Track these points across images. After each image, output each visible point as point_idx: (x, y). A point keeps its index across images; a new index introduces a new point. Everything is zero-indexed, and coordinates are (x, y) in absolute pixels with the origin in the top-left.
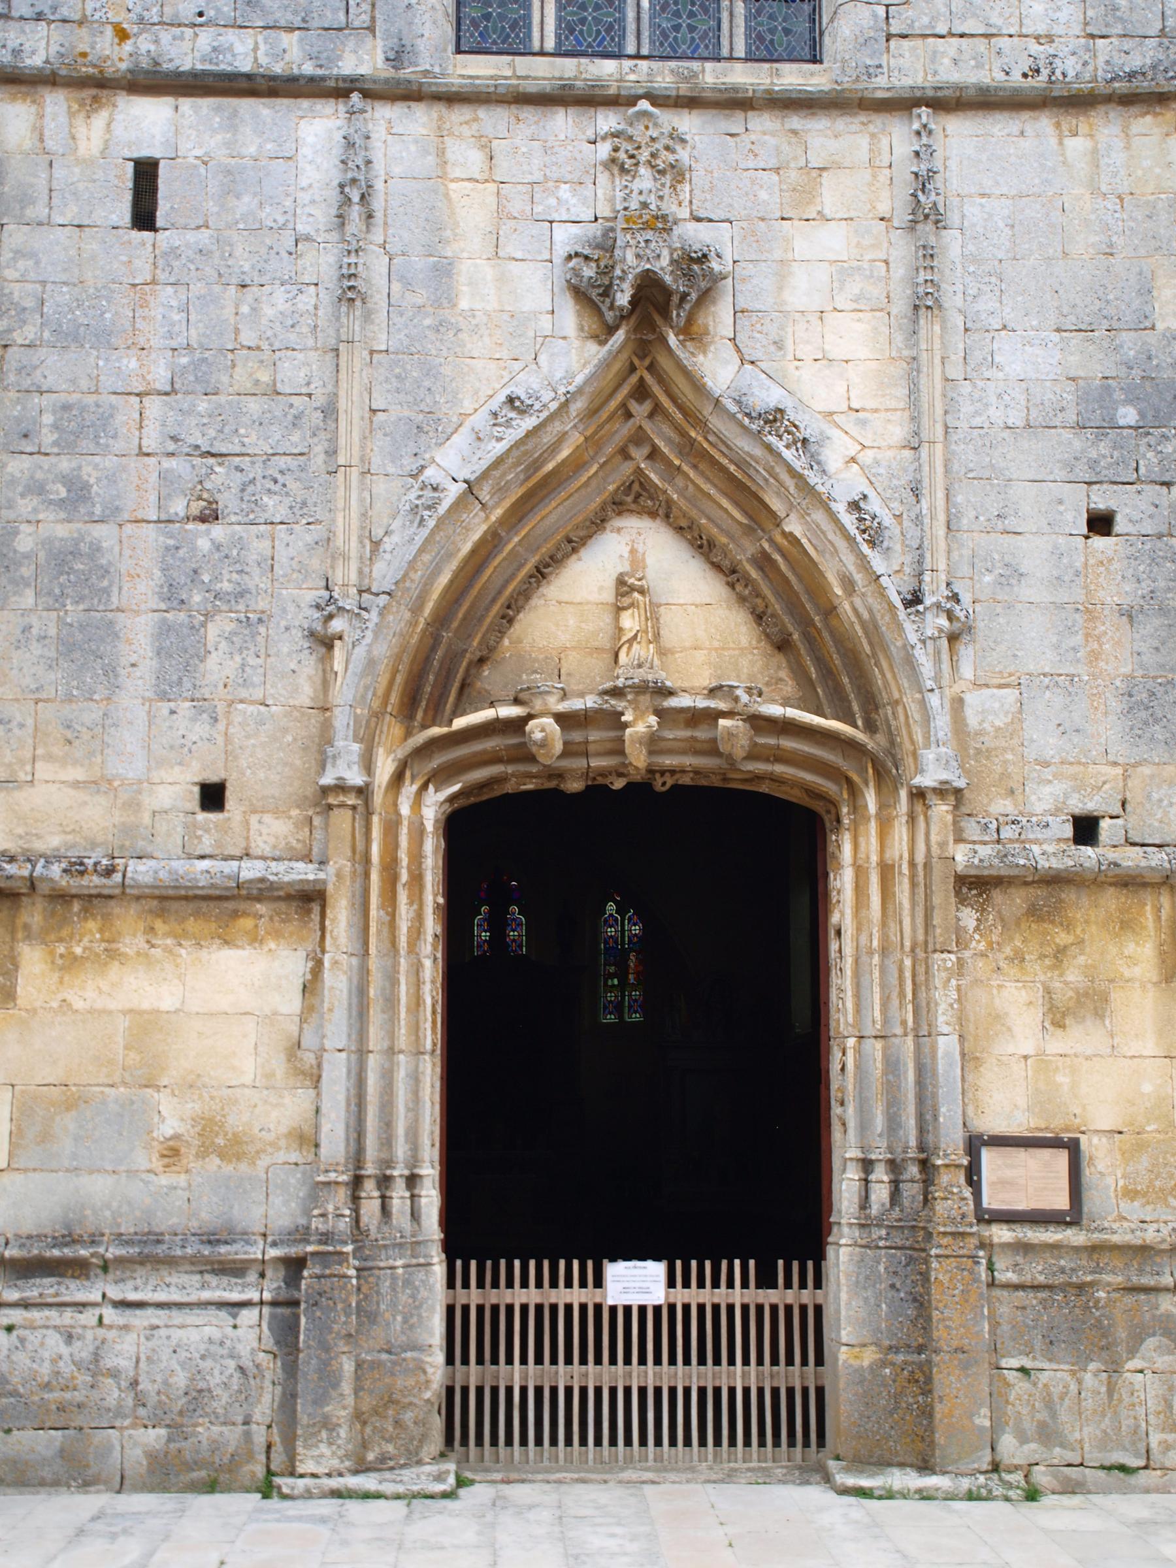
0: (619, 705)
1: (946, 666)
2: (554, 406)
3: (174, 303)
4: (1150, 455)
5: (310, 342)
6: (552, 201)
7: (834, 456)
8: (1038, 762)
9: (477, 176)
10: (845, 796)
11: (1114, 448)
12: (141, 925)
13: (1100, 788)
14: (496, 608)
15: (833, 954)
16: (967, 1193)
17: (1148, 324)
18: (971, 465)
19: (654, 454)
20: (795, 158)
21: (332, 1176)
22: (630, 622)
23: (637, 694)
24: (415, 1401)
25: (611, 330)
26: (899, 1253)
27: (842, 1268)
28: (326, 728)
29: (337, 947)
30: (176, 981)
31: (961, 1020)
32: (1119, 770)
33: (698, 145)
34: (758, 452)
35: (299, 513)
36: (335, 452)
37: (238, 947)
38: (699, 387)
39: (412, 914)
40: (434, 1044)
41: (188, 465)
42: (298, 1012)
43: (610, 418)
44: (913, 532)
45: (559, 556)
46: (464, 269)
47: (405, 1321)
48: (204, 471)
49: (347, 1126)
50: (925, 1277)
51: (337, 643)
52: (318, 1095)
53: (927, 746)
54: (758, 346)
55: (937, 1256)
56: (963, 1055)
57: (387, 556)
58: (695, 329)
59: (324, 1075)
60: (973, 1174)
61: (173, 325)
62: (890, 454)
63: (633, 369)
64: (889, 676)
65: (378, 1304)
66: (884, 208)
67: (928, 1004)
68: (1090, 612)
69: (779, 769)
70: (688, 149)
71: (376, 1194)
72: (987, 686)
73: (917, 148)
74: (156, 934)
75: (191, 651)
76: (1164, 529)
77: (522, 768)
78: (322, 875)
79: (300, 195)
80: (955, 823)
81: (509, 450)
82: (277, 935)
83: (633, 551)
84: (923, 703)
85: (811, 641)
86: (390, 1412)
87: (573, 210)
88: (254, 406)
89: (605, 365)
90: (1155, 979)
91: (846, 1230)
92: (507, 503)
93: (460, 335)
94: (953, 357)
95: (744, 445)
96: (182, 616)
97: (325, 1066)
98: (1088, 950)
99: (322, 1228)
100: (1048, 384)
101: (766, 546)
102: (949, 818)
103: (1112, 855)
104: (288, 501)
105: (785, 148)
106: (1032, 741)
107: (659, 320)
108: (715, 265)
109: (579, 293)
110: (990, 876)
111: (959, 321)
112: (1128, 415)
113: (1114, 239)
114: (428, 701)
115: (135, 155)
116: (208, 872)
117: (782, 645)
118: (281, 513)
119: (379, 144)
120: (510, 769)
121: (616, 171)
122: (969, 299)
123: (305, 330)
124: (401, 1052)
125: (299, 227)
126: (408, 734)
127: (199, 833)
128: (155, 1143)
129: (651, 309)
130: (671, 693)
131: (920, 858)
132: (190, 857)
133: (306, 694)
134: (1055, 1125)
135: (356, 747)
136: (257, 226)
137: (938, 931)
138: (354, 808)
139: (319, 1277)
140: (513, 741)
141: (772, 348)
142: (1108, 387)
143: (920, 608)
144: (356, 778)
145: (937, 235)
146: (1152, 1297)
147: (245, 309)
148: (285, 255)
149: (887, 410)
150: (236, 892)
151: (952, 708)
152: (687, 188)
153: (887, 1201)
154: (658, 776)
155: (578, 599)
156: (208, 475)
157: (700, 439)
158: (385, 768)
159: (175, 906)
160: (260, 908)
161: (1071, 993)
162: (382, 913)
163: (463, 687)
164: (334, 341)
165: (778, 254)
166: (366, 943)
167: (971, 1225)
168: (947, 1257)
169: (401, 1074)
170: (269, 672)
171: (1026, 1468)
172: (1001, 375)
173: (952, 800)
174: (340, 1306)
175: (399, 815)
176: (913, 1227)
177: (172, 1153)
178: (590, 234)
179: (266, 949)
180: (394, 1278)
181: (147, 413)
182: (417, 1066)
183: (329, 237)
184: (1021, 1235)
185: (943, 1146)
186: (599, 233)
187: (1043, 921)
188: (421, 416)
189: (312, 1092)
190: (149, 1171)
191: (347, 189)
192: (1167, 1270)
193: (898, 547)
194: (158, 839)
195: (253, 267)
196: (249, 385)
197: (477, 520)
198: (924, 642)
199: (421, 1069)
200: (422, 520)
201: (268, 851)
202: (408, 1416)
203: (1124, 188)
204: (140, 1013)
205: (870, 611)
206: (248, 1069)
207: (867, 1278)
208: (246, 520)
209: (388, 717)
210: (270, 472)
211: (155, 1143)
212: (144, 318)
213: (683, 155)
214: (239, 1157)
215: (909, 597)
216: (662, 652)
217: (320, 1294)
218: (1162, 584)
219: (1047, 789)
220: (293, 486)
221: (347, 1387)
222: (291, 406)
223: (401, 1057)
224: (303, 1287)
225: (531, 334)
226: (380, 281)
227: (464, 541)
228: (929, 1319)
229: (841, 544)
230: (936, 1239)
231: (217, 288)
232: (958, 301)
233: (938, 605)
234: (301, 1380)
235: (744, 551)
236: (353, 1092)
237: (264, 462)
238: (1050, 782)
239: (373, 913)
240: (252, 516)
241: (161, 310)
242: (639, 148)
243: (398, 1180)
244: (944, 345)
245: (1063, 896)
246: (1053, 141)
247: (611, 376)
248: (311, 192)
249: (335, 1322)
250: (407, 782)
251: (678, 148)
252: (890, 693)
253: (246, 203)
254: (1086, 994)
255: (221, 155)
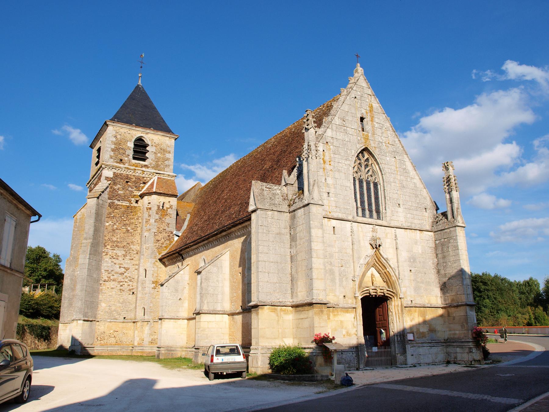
88: (345, 254)
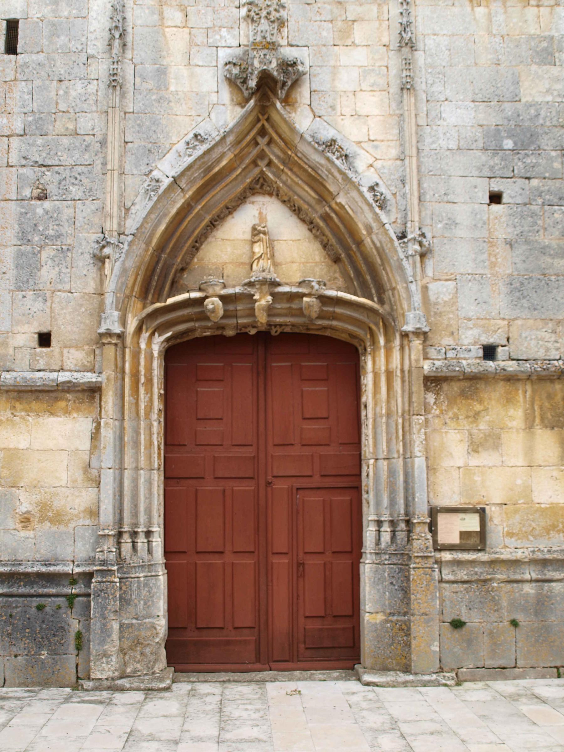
0: (252, 291)
1: (419, 269)
2: (218, 138)
3: (26, 90)
4: (520, 164)
5: (94, 108)
6: (218, 37)
7: (361, 164)
8: (465, 318)
9: (179, 25)
10: (369, 337)
11: (502, 160)
12: (9, 405)
13: (496, 331)
14: (189, 242)
15: (363, 417)
16: (429, 536)
17: (517, 99)
18: (431, 169)
19: (270, 164)
20: (340, 16)
21: (106, 532)
22: (258, 249)
23: (261, 285)
24: (151, 643)
25: (247, 100)
26: (395, 567)
27: (366, 574)
28: (102, 304)
29: (108, 416)
30: (27, 434)
31: (427, 450)
32: (506, 322)
33: (291, 9)
34: (323, 161)
35: (88, 194)
36: (106, 164)
37: (58, 416)
38: (292, 129)
39: (147, 399)
40: (159, 465)
41: (32, 172)
42: (89, 449)
43: (247, 145)
44: (402, 202)
45: (222, 216)
46: (172, 71)
47: (145, 604)
48: (40, 174)
49: (114, 507)
50: (408, 578)
51: (107, 260)
52: (99, 491)
53: (409, 311)
54: (322, 108)
55: (414, 568)
56: (428, 467)
57: (133, 216)
58: (290, 100)
59: (102, 481)
60: (433, 527)
61: (25, 101)
62: (390, 163)
63: (259, 120)
64: (390, 275)
65: (131, 595)
66: (385, 40)
67: (410, 441)
68: (490, 242)
69: (334, 323)
70: (286, 11)
71: (130, 540)
72: (440, 280)
73: (401, 11)
74: (16, 410)
75: (33, 266)
76: (527, 201)
77: (203, 324)
78: (99, 379)
79: (90, 35)
80: (424, 349)
81: (195, 161)
82: (78, 410)
83: (260, 213)
84: (407, 289)
85: (350, 257)
86: (138, 649)
87: (228, 41)
88: (65, 141)
89: (244, 118)
90: (523, 428)
91: (369, 556)
92: (194, 188)
93: (170, 104)
94: (421, 115)
95: (316, 158)
96: (29, 248)
97: (102, 476)
98: (490, 413)
99: (102, 558)
100: (469, 128)
101: (328, 209)
102: (421, 347)
103: (502, 364)
104: (82, 189)
105: (335, 11)
106: (463, 308)
107: (270, 93)
108: (300, 68)
109: (231, 81)
110: (441, 376)
111: (424, 97)
112: (509, 144)
113: (500, 57)
114: (155, 289)
115: (7, 17)
116: (42, 378)
117: (337, 260)
118: (79, 195)
119: (130, 10)
120: (197, 324)
121: (250, 21)
122: (429, 85)
123: (91, 102)
124: (142, 469)
125: (89, 51)
126: (144, 307)
127: (38, 358)
128: (18, 515)
129: (267, 90)
130: (279, 285)
131: (406, 368)
132: (33, 370)
133: (91, 287)
134: (474, 501)
135: (116, 314)
136: (68, 51)
137: (415, 404)
138: (116, 345)
139: (100, 582)
140: (197, 310)
141: (330, 110)
142: (499, 130)
143: (406, 240)
144: (117, 329)
145: (412, 54)
146: (520, 585)
147: (61, 92)
148: (82, 65)
149: (388, 141)
150: (56, 388)
151: (422, 291)
152: (286, 30)
153: (389, 541)
154: (273, 327)
155: (232, 238)
156: (42, 176)
157: (293, 155)
158: (132, 324)
159: (26, 395)
160: (69, 396)
161: (482, 435)
162: (131, 398)
163: (173, 283)
164: (106, 108)
165: (332, 63)
166: (123, 414)
167: (431, 552)
168: (419, 568)
169: (142, 480)
170: (73, 276)
171: (456, 670)
172: (445, 123)
173: (422, 337)
174: (111, 597)
175: (139, 347)
176: (402, 554)
177: (26, 520)
178: (237, 53)
179: (72, 417)
180: (139, 582)
181: (12, 145)
182: (150, 476)
183: (104, 56)
184: (456, 556)
185: (417, 513)
186: (241, 53)
187: (468, 399)
188: (150, 145)
189: (96, 490)
190: (15, 529)
191: (113, 32)
192: (527, 572)
193: (394, 210)
194: (17, 362)
195: (65, 71)
196: (63, 130)
197: (179, 197)
198: (407, 257)
199: (152, 477)
200: (150, 197)
201: (73, 367)
202: (148, 650)
203: (504, 32)
204: (9, 450)
205: (380, 242)
206: (64, 478)
207: (379, 579)
208: (61, 198)
209: (133, 298)
210: (73, 174)
211: (18, 515)
212: (10, 98)
213: (283, 13)
214: (60, 522)
215: (400, 235)
216: (275, 264)
217: (101, 591)
218: (526, 228)
219: (470, 332)
220: (85, 181)
221: (115, 636)
222: (84, 140)
223: (142, 471)
224: (92, 587)
225: (207, 103)
226: (129, 77)
227: (173, 208)
228: (409, 599)
229: (366, 208)
230: (413, 560)
231: (47, 82)
232: (423, 86)
233: (414, 239)
234: (92, 633)
235: (317, 212)
236: (117, 489)
237: (70, 169)
238: (471, 328)
239: (127, 398)
240: (64, 197)
241: (19, 93)
242: (261, 10)
243: (141, 534)
244: (416, 108)
245: (478, 386)
246: (469, 9)
247: (247, 124)
248: (95, 33)
249: (109, 604)
250: (144, 331)
251: (281, 10)
252: (390, 283)
253: (63, 39)
254: (489, 435)
255: (50, 16)
